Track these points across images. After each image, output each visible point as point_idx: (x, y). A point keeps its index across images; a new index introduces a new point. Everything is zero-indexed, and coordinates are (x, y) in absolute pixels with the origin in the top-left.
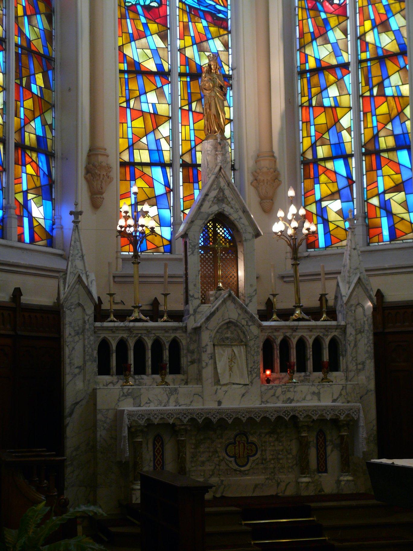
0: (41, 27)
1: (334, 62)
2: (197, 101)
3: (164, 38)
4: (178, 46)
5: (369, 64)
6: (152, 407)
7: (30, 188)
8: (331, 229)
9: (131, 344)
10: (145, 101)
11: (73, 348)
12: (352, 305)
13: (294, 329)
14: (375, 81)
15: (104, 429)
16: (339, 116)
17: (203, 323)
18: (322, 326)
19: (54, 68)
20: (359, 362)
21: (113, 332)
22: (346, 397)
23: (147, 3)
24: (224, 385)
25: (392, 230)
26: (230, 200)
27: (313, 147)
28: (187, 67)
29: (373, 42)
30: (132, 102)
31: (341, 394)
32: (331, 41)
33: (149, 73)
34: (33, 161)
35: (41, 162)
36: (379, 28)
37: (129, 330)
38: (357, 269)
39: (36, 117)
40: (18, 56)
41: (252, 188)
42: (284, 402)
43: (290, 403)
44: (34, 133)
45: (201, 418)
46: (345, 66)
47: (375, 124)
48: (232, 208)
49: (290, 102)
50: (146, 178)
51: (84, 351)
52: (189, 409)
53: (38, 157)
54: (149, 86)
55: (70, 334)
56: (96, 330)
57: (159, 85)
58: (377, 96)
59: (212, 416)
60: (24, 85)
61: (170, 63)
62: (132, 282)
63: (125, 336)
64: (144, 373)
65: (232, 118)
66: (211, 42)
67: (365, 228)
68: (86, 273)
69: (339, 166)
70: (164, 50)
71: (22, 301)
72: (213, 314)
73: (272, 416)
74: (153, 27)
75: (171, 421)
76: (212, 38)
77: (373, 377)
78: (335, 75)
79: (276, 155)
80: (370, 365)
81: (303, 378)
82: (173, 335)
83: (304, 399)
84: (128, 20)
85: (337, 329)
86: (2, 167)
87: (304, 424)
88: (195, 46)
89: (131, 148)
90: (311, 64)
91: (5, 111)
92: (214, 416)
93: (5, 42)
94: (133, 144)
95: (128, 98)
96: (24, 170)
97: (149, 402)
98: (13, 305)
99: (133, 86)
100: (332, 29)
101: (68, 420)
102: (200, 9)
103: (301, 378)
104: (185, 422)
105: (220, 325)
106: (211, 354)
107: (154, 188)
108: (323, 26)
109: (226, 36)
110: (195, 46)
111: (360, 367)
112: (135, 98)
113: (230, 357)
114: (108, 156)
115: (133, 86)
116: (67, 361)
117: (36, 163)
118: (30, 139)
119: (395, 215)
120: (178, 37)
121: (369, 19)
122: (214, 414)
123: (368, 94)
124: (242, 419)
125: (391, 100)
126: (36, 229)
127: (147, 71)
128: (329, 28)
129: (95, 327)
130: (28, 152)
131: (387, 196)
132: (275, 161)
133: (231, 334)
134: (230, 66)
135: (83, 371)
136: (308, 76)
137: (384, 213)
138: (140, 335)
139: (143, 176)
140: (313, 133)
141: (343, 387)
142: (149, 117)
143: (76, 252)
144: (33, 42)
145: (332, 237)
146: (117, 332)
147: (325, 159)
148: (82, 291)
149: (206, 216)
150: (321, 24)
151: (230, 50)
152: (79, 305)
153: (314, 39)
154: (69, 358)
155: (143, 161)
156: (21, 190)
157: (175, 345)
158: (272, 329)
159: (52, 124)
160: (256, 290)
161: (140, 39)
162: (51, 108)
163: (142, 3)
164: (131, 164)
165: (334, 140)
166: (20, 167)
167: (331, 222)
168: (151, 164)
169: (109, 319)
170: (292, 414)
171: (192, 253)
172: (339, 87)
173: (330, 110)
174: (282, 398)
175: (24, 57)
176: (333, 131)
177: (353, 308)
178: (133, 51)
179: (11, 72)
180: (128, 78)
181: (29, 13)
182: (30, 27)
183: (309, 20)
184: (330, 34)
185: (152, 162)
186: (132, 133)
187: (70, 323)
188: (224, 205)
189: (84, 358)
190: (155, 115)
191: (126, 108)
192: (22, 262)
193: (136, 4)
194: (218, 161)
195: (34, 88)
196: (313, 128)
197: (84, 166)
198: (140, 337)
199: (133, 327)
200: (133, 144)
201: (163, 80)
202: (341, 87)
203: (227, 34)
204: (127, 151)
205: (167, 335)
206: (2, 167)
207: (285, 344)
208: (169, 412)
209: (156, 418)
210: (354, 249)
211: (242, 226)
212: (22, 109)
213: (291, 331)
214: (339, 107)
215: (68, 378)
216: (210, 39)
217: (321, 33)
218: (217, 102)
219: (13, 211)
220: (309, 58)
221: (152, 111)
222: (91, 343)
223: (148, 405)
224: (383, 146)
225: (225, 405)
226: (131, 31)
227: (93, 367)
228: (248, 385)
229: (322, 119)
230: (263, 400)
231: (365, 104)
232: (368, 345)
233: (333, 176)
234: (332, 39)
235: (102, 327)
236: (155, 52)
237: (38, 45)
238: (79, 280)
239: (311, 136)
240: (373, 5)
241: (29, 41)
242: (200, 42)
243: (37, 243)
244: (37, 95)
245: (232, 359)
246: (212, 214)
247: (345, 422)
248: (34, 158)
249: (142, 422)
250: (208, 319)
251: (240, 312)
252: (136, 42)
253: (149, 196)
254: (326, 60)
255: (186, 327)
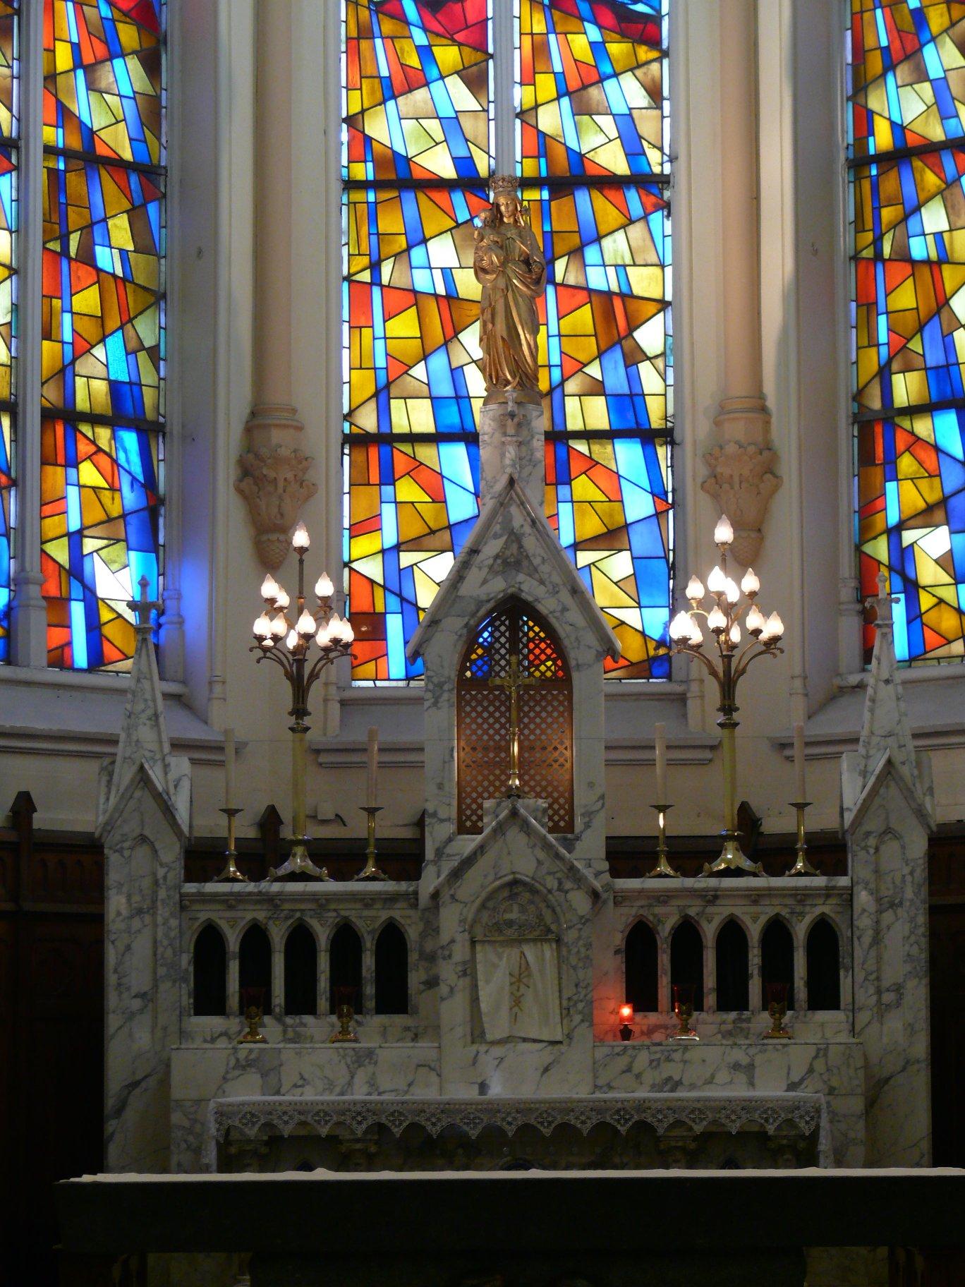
0: (126, 90)
1: (936, 133)
2: (569, 254)
3: (475, 81)
4: (517, 103)
6: (309, 1095)
7: (87, 522)
8: (923, 610)
9: (278, 936)
10: (423, 262)
11: (128, 948)
12: (868, 834)
13: (712, 897)
15: (189, 1147)
16: (949, 288)
17: (442, 885)
18: (783, 889)
19: (164, 196)
20: (886, 983)
21: (231, 907)
22: (825, 1077)
24: (493, 1043)
26: (537, 561)
27: (884, 374)
28: (543, 161)
30: (386, 268)
31: (811, 1071)
33: (436, 184)
34: (99, 450)
35: (125, 451)
37: (270, 901)
38: (890, 735)
39: (108, 331)
41: (703, 496)
42: (654, 1087)
43: (672, 1090)
44: (104, 375)
45: (400, 1124)
48: (542, 582)
50: (423, 475)
51: (155, 954)
52: (371, 1103)
53: (114, 437)
54: (434, 221)
55: (119, 914)
56: (184, 904)
57: (463, 216)
59: (428, 1119)
60: (73, 253)
61: (493, 153)
62: (362, 766)
63: (261, 916)
64: (312, 1010)
65: (669, 297)
66: (610, 85)
68: (164, 759)
70: (476, 118)
71: (35, 826)
72: (468, 862)
73: (583, 1122)
74: (448, 55)
75: (324, 1131)
76: (616, 75)
77: (923, 1025)
78: (939, 170)
79: (771, 403)
80: (917, 995)
81: (730, 1027)
82: (384, 915)
83: (710, 1081)
84: (378, 42)
85: (828, 896)
86: (8, 475)
87: (673, 1144)
88: (565, 101)
89: (383, 396)
90: (882, 138)
91: (15, 330)
92: (434, 1120)
93: (18, 148)
94: (388, 385)
95: (375, 257)
96: (73, 478)
97: (303, 1082)
98: (12, 837)
99: (390, 222)
100: (933, 39)
101: (111, 1125)
103: (724, 1027)
104: (359, 1133)
105: (489, 889)
106: (464, 963)
107: (445, 502)
108: (913, 30)
109: (655, 67)
110: (565, 101)
111: (888, 997)
112: (395, 255)
113: (516, 973)
114: (299, 428)
116: (111, 979)
117: (109, 455)
118: (90, 391)
120: (517, 78)
122: (433, 1115)
124: (506, 1127)
127: (430, 180)
128: (927, 36)
129: (181, 895)
130: (86, 429)
132: (768, 423)
133: (520, 913)
134: (667, 150)
135: (150, 1005)
136: (874, 172)
138: (298, 915)
139: (416, 469)
140: (883, 337)
141: (819, 1050)
142: (432, 306)
143: (142, 706)
144: (102, 134)
145: (928, 633)
146: (240, 907)
148: (150, 804)
149: (473, 607)
150: (907, 23)
151: (666, 104)
152: (143, 839)
154: (115, 971)
155: (417, 429)
156: (63, 531)
157: (825, 940)
158: (648, 898)
160: (602, 797)
161: (410, 91)
164: (386, 439)
165: (935, 358)
166: (60, 470)
167: (923, 588)
169: (287, 867)
170: (636, 1118)
171: (435, 704)
172: (949, 205)
173: (926, 271)
174: (650, 1077)
175: (75, 182)
177: (872, 841)
178: (385, 128)
179: (31, 231)
180: (376, 203)
181: (88, 58)
183: (879, 12)
184: (929, 52)
185: (442, 430)
186: (387, 355)
187: (121, 885)
188: (521, 577)
189: (155, 972)
190: (451, 298)
191: (371, 284)
192: (41, 725)
194: (507, 462)
195: (106, 258)
196: (882, 320)
197: (234, 457)
198: (300, 919)
199: (280, 894)
200: (388, 385)
201: (474, 200)
202: (953, 207)
203: (659, 60)
205: (366, 913)
206: (8, 475)
207: (687, 933)
208: (320, 1107)
209: (286, 1123)
210: (887, 682)
211: (568, 628)
213: (699, 902)
214: (948, 262)
215: (113, 1022)
216: (609, 77)
218: (512, 304)
219: (34, 591)
220: (877, 120)
221: (441, 291)
222: (173, 934)
223: (299, 1090)
225: (497, 1090)
226: (384, 72)
227: (180, 993)
228: (561, 1042)
229: (905, 297)
230: (600, 1082)
232: (913, 939)
233: (930, 459)
235: (200, 894)
236: (453, 124)
237: (119, 142)
238: (142, 777)
239: (878, 345)
241: (90, 135)
242: (579, 92)
243: (110, 668)
245: (521, 976)
246: (488, 601)
247: (785, 1142)
249: (252, 1132)
250: (456, 874)
251: (542, 855)
252: (400, 99)
253: (431, 524)
254: (918, 127)
255: (416, 893)
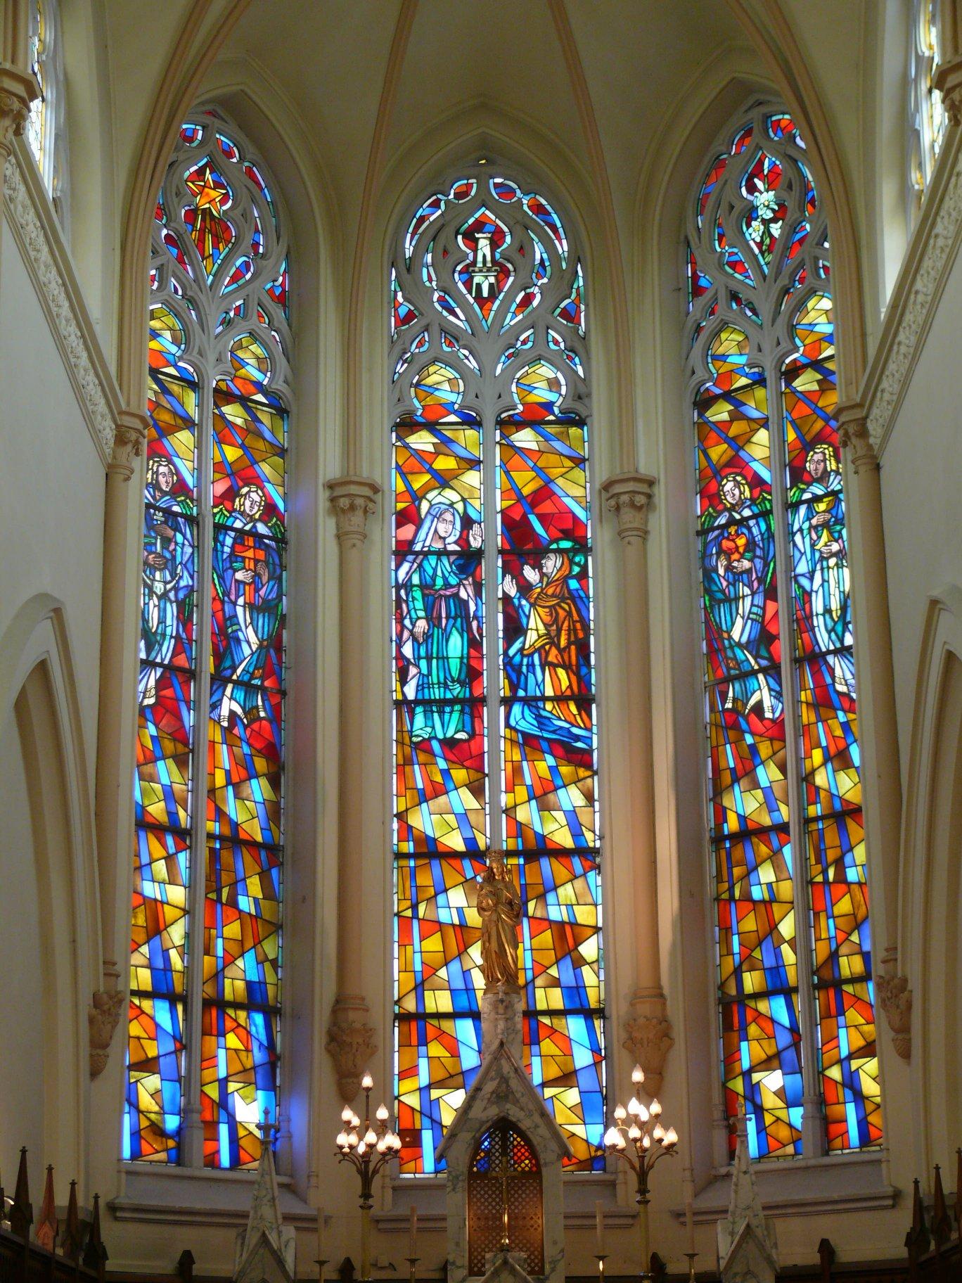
1: (766, 821)
3: (477, 791)
5: (821, 826)
12: (736, 1274)
14: (831, 855)
16: (777, 917)
19: (282, 864)
23: (449, 735)
25: (863, 1124)
27: (738, 973)
29: (826, 786)
30: (422, 908)
32: (763, 785)
33: (453, 855)
34: (239, 1025)
36: (835, 762)
38: (748, 1208)
40: (214, 855)
46: (782, 828)
47: (832, 933)
48: (522, 1109)
49: (692, 895)
53: (248, 1017)
54: (452, 877)
58: (835, 882)
62: (407, 1230)
65: (600, 925)
66: (561, 792)
67: (818, 1122)
69: (777, 1008)
71: (194, 1273)
74: (460, 774)
76: (565, 786)
78: (768, 844)
79: (666, 991)
84: (416, 767)
88: (533, 802)
89: (419, 989)
90: (732, 824)
94: (423, 982)
99: (424, 879)
100: (762, 763)
102: (542, 738)
110: (533, 802)
115: (424, 879)
117: (245, 1028)
118: (234, 987)
119: (867, 1098)
120: (503, 788)
121: (819, 745)
123: (819, 879)
125: (855, 888)
126: (243, 1143)
130: (231, 1012)
131: (855, 1064)
132: (664, 1004)
136: (728, 845)
137: (849, 1093)
139: (442, 1036)
140: (736, 949)
143: (264, 1193)
144: (244, 826)
147: (756, 996)
150: (746, 753)
151: (597, 804)
153: (736, 780)
155: (442, 1010)
159: (277, 959)
160: (562, 1251)
162: (276, 931)
163: (440, 736)
164: (421, 1017)
165: (769, 962)
168: (455, 1015)
173: (762, 908)
175: (226, 856)
176: (767, 945)
178: (424, 820)
181: (235, 779)
182: (239, 802)
184: (760, 771)
188: (508, 1106)
190: (462, 927)
192: (198, 1206)
193: (430, 739)
194: (499, 1031)
195: (245, 904)
196: (735, 939)
197: (324, 1030)
200: (423, 982)
201: (476, 864)
203: (592, 777)
204: (413, 994)
210: (745, 1173)
211: (539, 1139)
212: (220, 941)
217: (745, 772)
221: (456, 922)
224: (846, 972)
226: (420, 786)
231: (814, 897)
233: (768, 1027)
234: (764, 782)
238: (264, 1240)
240: (824, 721)
241: (235, 826)
242: (543, 796)
244: (250, 914)
248: (242, 1022)
254: (754, 817)
